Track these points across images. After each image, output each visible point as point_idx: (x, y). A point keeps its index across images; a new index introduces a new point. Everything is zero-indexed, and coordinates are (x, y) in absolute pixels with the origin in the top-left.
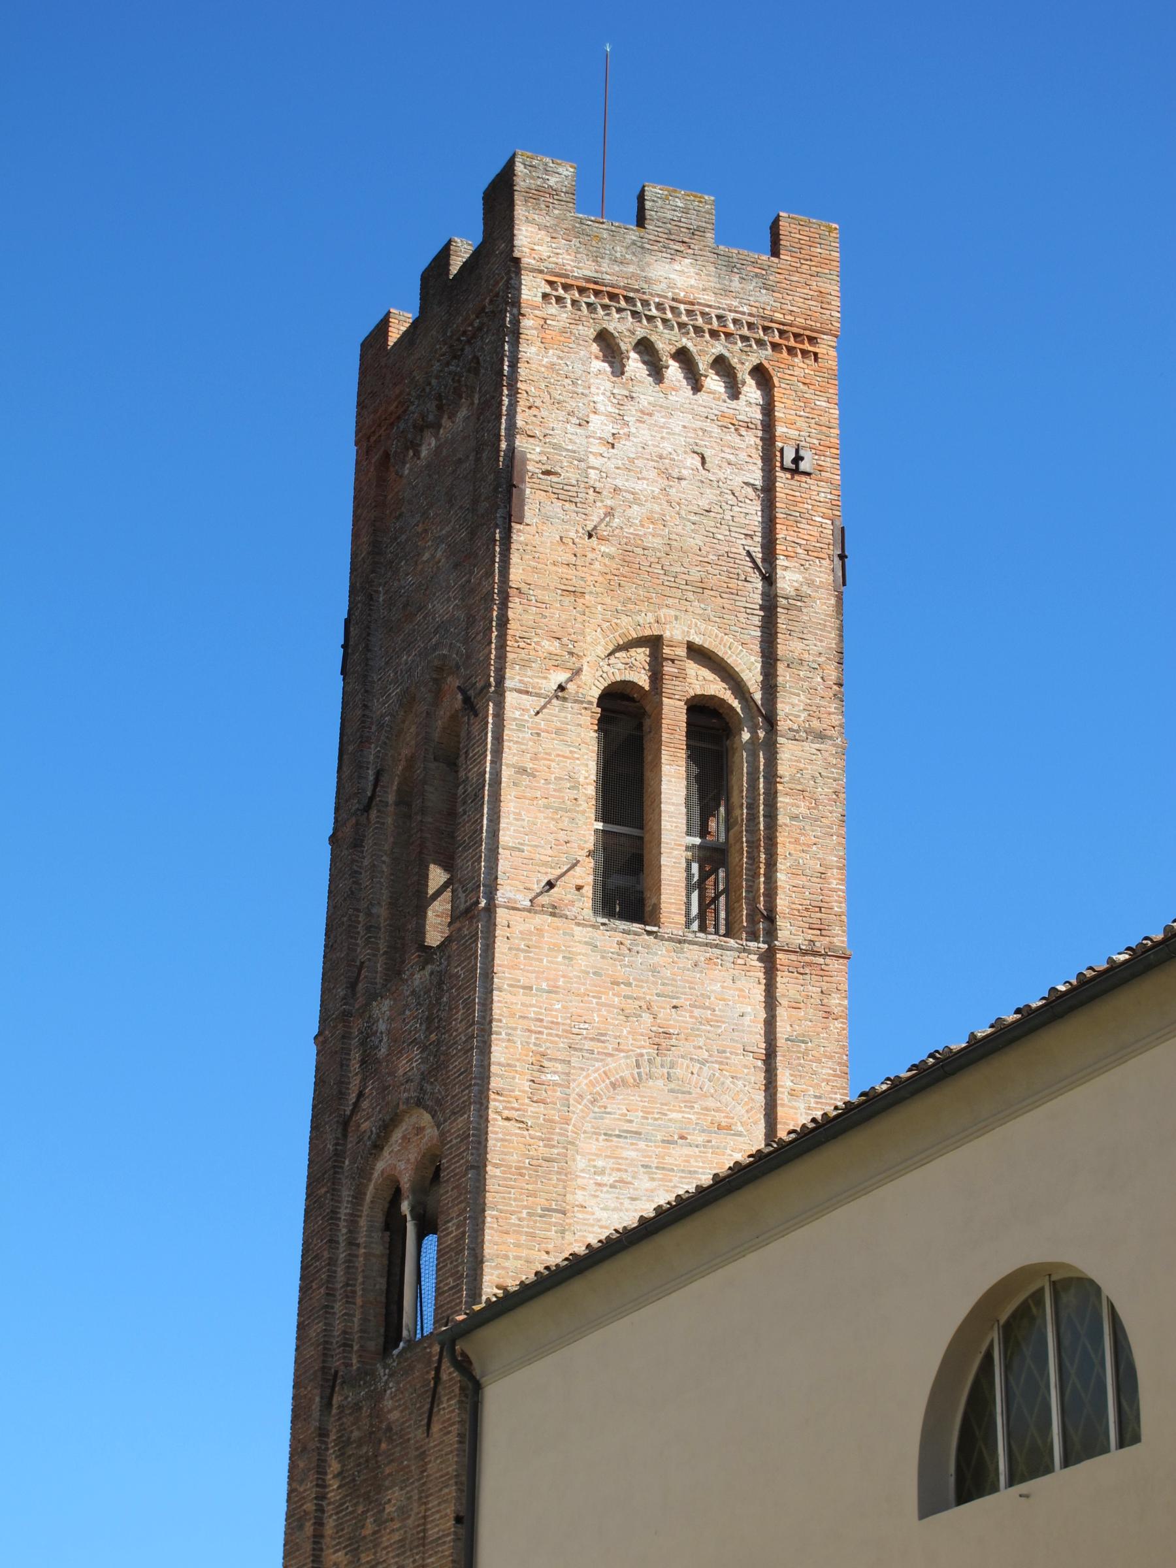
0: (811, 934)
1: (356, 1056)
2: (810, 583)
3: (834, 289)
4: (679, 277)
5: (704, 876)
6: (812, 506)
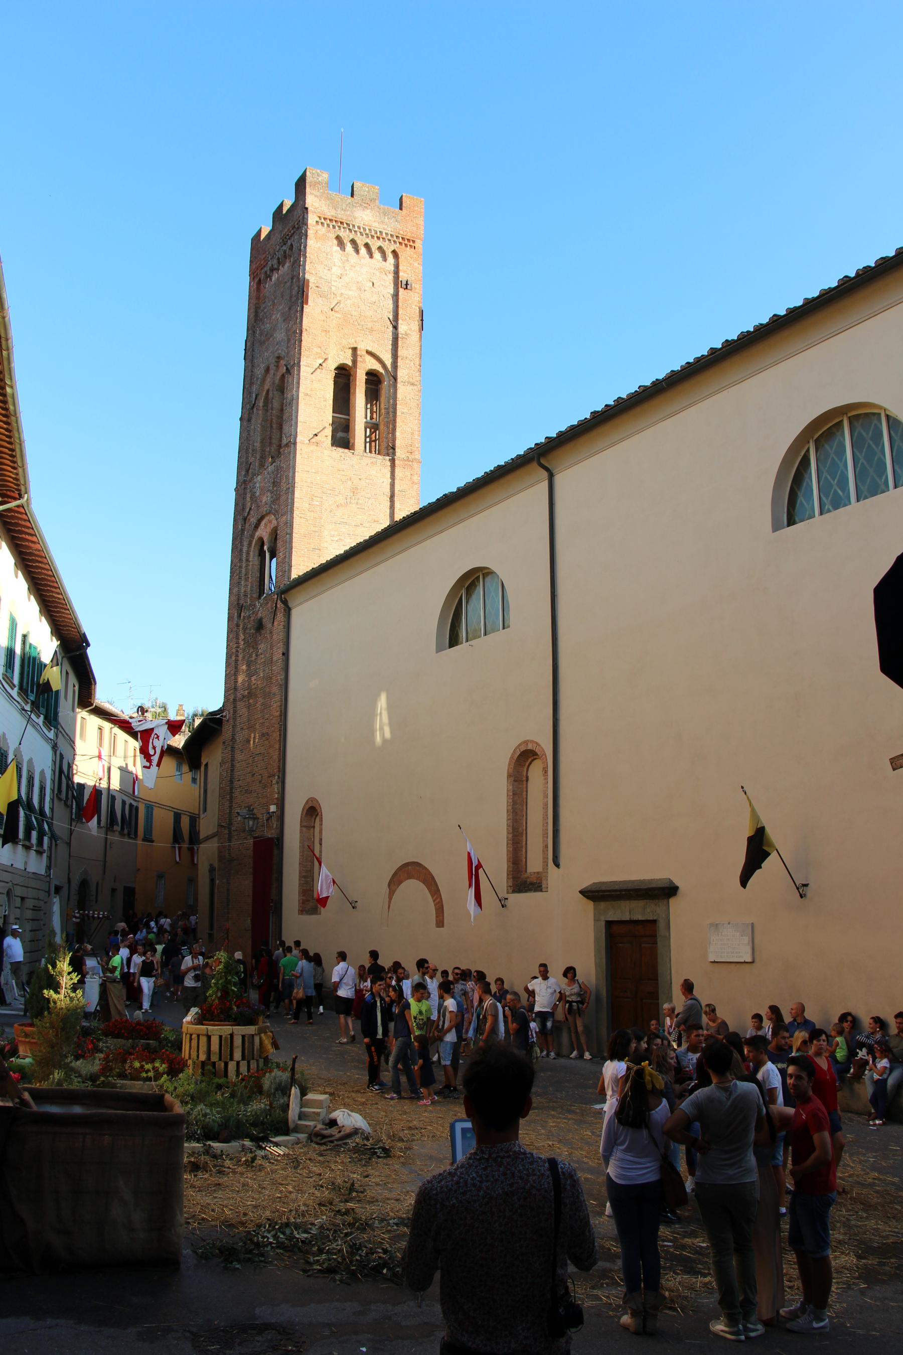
0: (408, 454)
1: (248, 495)
2: (411, 330)
3: (422, 223)
4: (365, 217)
5: (371, 433)
6: (410, 301)
